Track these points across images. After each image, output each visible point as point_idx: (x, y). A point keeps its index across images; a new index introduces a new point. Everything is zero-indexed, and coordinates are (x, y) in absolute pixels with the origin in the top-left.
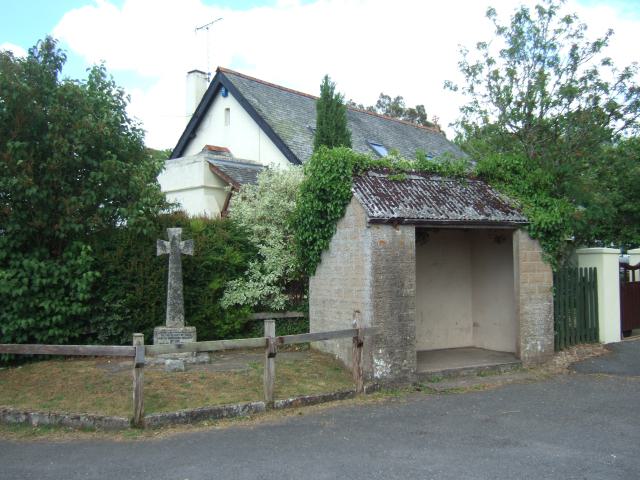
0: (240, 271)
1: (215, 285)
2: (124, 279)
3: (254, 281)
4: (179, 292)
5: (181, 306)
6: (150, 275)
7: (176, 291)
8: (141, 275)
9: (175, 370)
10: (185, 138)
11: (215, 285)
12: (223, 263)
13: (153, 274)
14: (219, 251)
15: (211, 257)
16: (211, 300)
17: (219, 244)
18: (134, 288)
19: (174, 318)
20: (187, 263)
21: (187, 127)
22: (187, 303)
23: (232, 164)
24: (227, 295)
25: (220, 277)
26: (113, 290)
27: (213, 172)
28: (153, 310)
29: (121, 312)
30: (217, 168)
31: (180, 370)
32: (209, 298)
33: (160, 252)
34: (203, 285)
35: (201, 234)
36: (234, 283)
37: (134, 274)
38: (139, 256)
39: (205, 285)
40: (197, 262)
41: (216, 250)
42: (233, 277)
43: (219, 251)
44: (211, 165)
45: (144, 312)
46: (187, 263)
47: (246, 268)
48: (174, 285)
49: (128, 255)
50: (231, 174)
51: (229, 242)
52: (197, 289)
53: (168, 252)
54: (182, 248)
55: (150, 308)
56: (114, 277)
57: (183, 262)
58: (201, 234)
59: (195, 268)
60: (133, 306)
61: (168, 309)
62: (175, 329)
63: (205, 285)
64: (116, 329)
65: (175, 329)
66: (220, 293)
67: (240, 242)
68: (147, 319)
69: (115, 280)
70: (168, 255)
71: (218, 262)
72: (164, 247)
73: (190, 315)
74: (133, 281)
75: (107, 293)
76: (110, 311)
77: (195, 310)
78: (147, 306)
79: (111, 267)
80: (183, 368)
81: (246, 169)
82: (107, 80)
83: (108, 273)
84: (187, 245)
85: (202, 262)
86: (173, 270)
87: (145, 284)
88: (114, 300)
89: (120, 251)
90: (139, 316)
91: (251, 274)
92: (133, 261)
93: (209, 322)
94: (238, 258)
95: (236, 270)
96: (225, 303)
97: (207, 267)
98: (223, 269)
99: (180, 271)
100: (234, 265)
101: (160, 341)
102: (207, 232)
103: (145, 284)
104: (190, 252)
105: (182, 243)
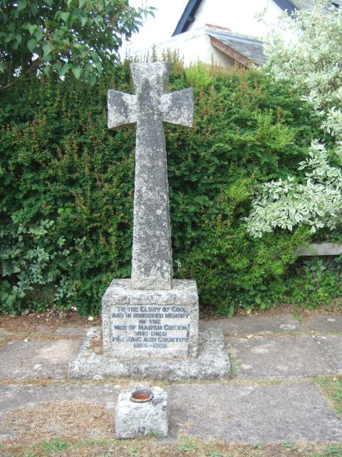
0: (291, 163)
1: (238, 191)
2: (53, 179)
3: (316, 182)
4: (159, 212)
5: (165, 243)
6: (105, 170)
7: (151, 209)
8: (87, 170)
9: (140, 435)
10: (184, 21)
11: (238, 191)
12: (253, 147)
13: (111, 168)
14: (243, 123)
15: (229, 134)
16: (228, 222)
17: (245, 111)
18: (72, 198)
19: (147, 271)
20: (178, 146)
21: (186, 9)
22: (178, 228)
23: (236, 40)
24: (260, 211)
25: (248, 174)
26: (32, 200)
27: (216, 49)
28: (113, 239)
29: (50, 244)
30: (220, 43)
31: (154, 435)
32: (225, 217)
33: (114, 119)
34: (212, 193)
35: (206, 90)
36: (275, 187)
37: (71, 169)
38: (81, 132)
39: (217, 191)
40: (201, 145)
41: (237, 121)
42: (270, 173)
43: (243, 123)
44: (213, 39)
45: (96, 242)
46: (178, 146)
47: (302, 157)
48: (145, 197)
49: (58, 132)
50: (237, 48)
51: (262, 106)
52: (200, 199)
53: (133, 118)
54: (164, 108)
55: (107, 235)
56: (30, 176)
57: (168, 145)
58: (206, 90)
59: (196, 158)
60: (73, 232)
61: (136, 248)
62: (149, 295)
63: (217, 191)
64: (44, 272)
65: (149, 295)
66: (244, 208)
67: (285, 106)
68: (79, 278)
69: (37, 182)
70: (133, 126)
71: (243, 145)
72: (124, 108)
73: (187, 247)
74: (72, 183)
75: (21, 207)
76: (29, 242)
77: (196, 242)
78: (100, 231)
79: (22, 156)
80: (164, 428)
81: (253, 45)
82: (134, 57)
83: (19, 168)
84: (176, 103)
85: (210, 145)
86: (146, 162)
87: (93, 188)
88: (36, 219)
89: (41, 122)
90: (87, 249)
91: (310, 169)
92: (68, 142)
93: (228, 283)
94: (284, 137)
95: (280, 162)
96: (257, 225)
97: (221, 155)
98: (253, 160)
99: (161, 163)
100: (275, 152)
101: (116, 322)
102: (218, 89)
103: (93, 188)
104: (185, 118)
105: (166, 99)
